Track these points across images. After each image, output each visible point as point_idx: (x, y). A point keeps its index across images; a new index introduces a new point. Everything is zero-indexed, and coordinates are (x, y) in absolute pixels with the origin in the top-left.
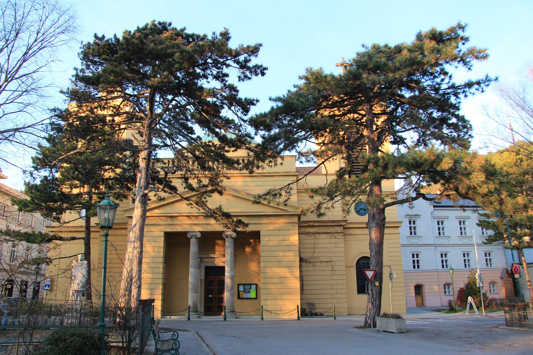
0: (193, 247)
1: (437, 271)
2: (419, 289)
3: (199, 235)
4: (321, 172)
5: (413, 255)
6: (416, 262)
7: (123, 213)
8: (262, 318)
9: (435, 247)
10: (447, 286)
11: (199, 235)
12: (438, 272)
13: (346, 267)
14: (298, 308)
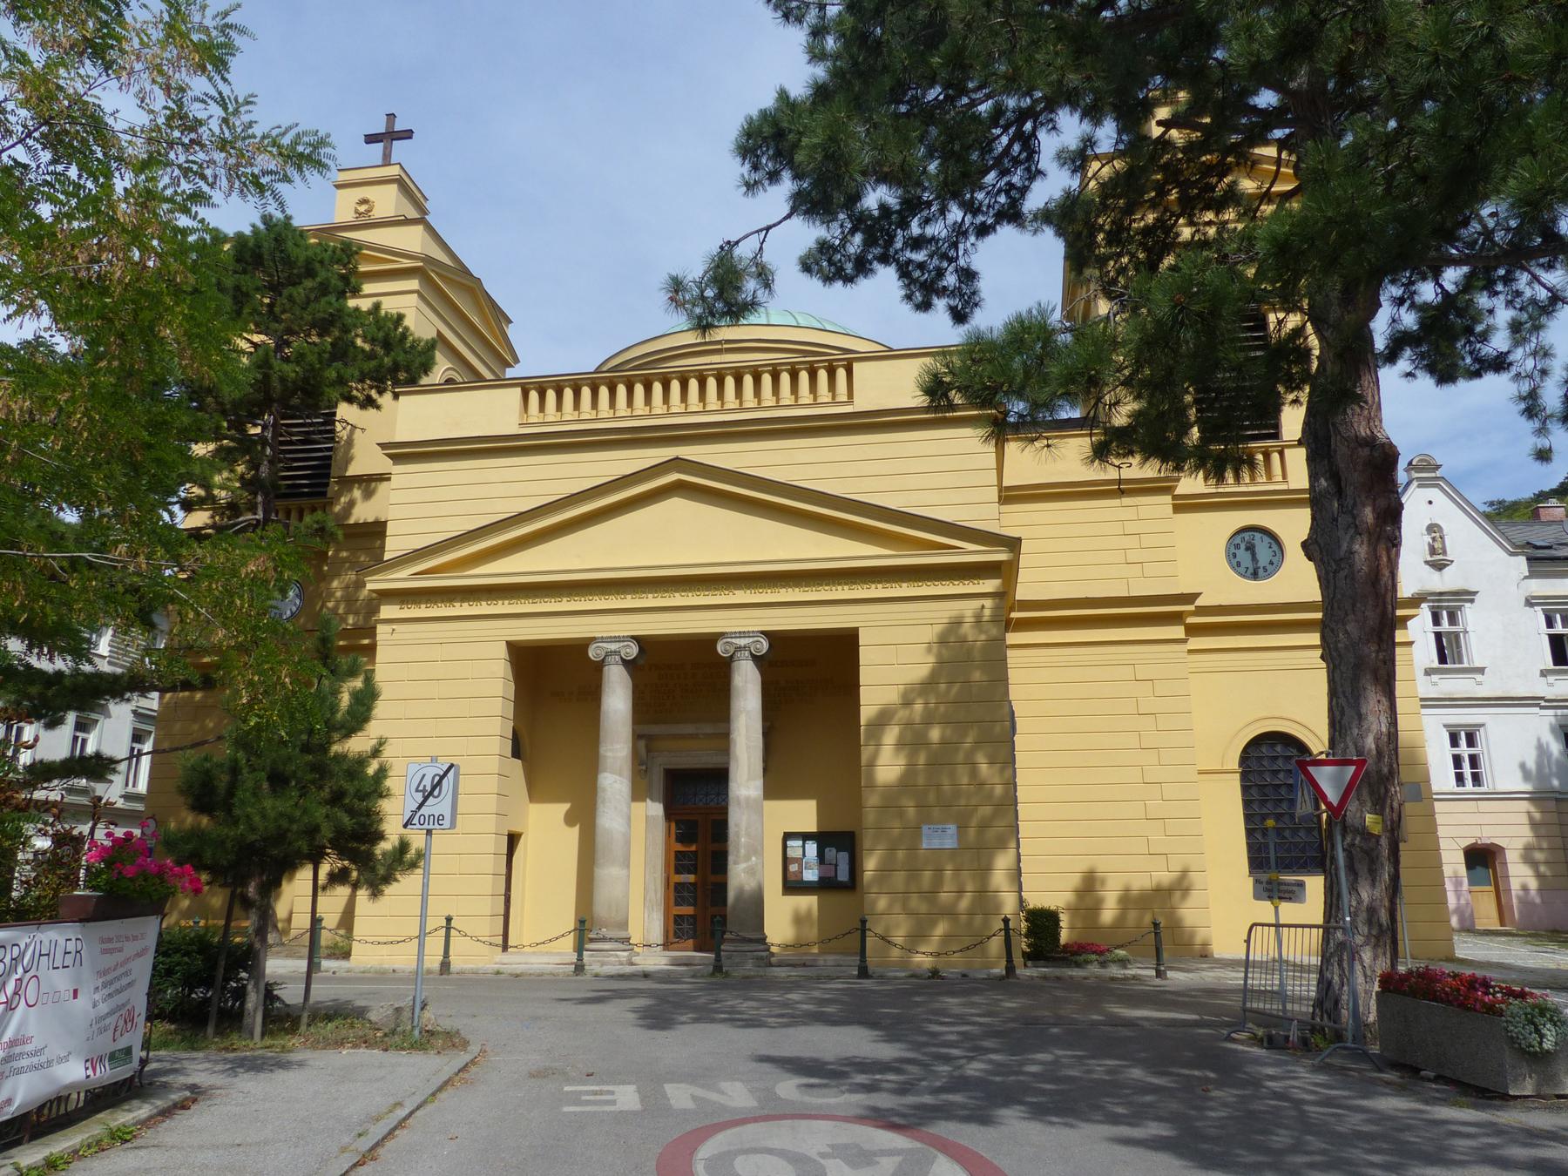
0: (617, 700)
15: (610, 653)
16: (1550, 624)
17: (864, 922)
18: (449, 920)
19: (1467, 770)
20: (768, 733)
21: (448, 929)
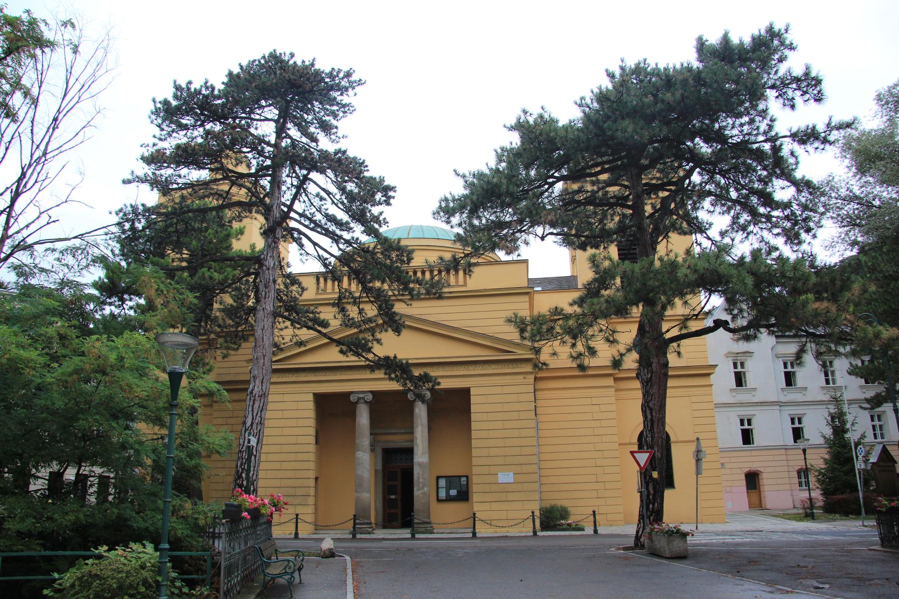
0: (363, 418)
1: (786, 448)
2: (752, 479)
3: (370, 397)
4: (577, 285)
5: (793, 421)
6: (878, 428)
7: (245, 364)
8: (474, 534)
9: (780, 406)
10: (802, 474)
11: (370, 397)
12: (786, 449)
13: (620, 444)
14: (533, 516)
15: (359, 399)
16: (785, 367)
17: (474, 514)
18: (297, 515)
19: (878, 432)
20: (430, 429)
21: (297, 519)
